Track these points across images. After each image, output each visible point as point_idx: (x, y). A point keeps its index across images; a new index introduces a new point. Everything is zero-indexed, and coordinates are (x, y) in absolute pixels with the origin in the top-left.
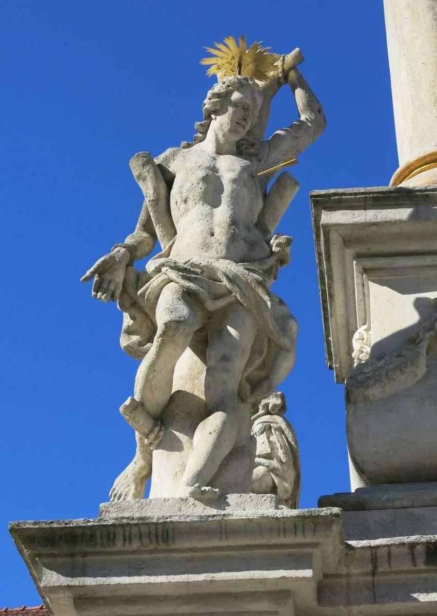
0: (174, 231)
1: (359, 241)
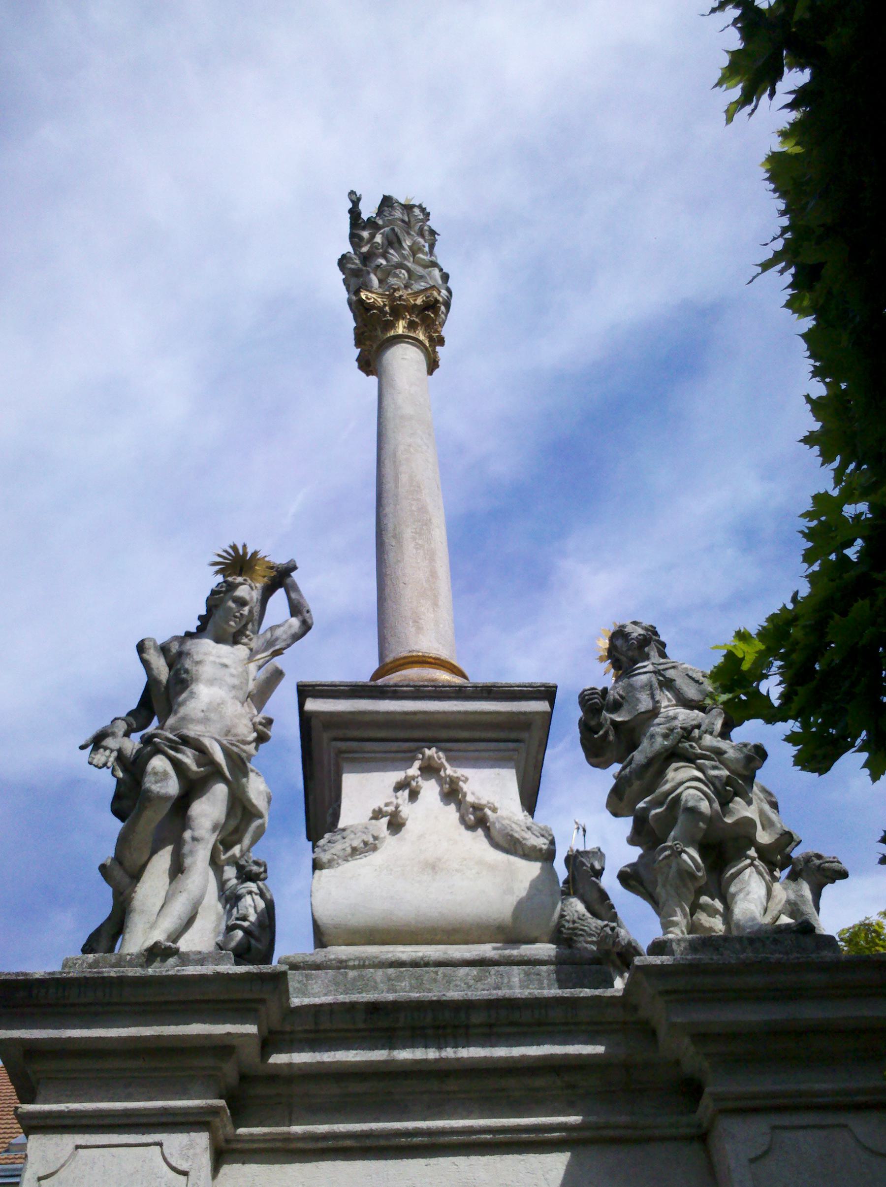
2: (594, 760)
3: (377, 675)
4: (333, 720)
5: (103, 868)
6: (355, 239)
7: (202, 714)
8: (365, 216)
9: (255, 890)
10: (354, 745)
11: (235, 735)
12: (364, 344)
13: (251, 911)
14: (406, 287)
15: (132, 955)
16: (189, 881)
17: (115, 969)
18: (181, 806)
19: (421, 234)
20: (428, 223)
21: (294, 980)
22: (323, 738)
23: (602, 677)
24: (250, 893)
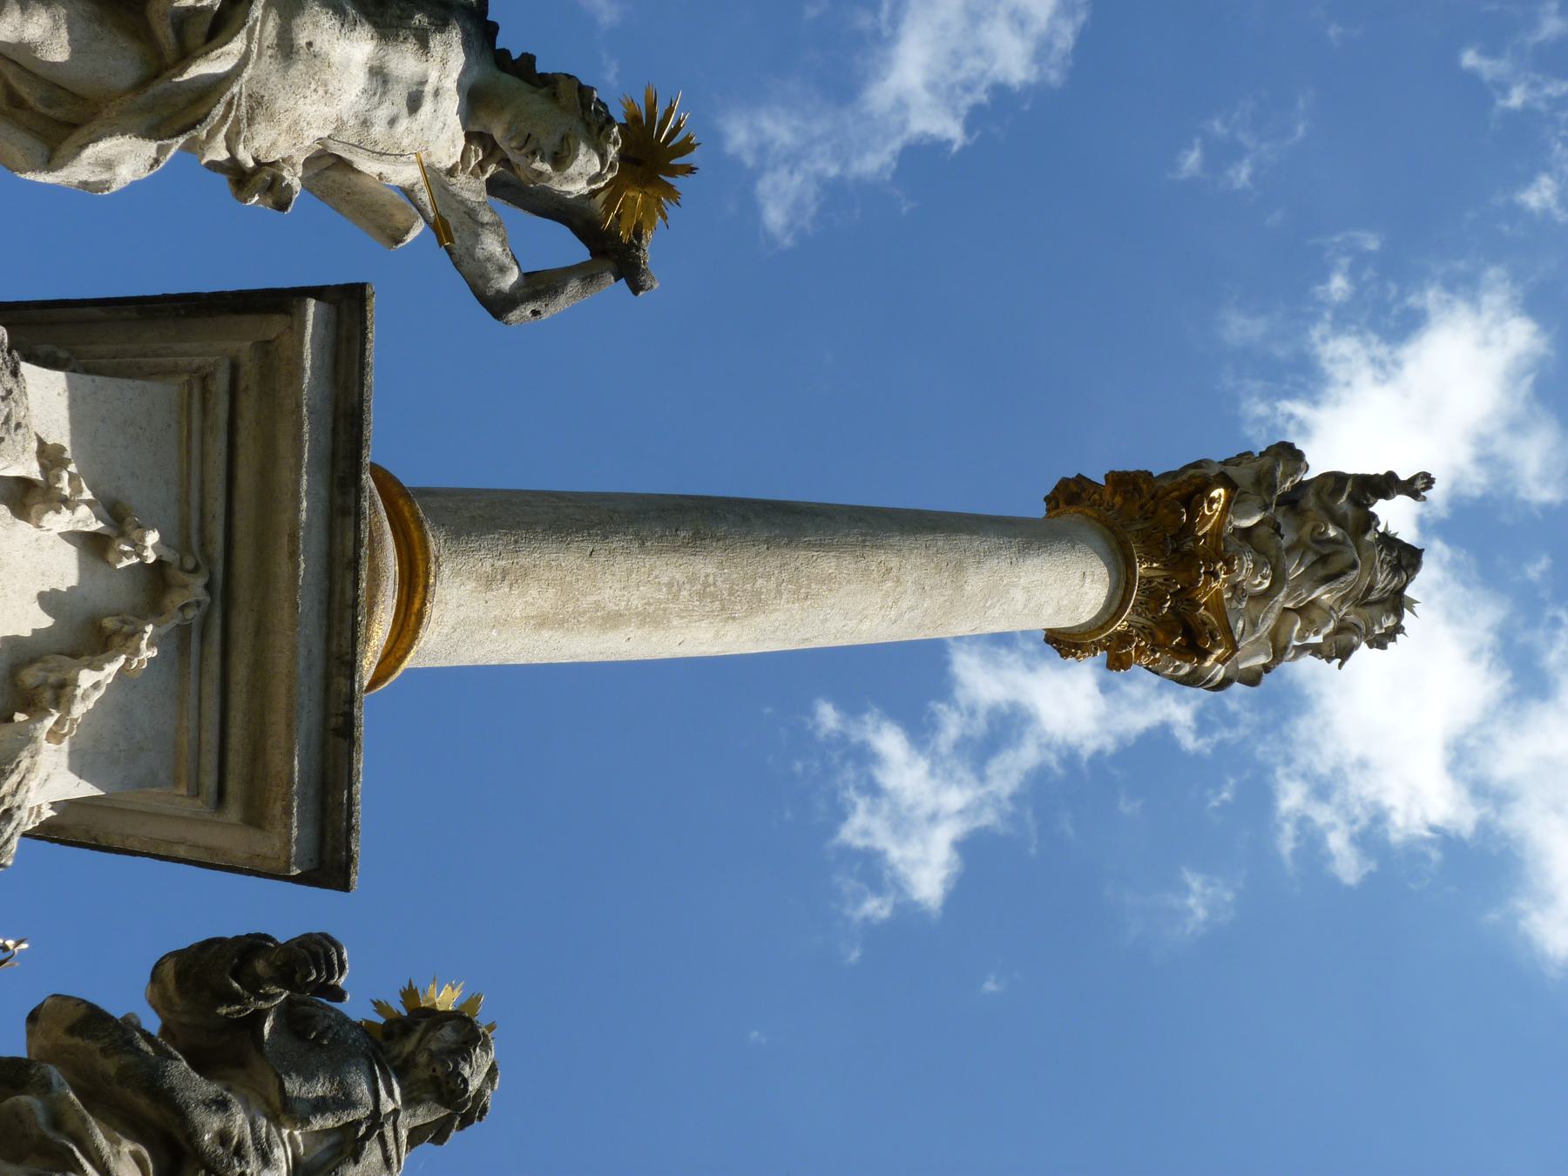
2: (169, 970)
3: (384, 480)
4: (275, 362)
6: (1335, 481)
7: (302, 40)
8: (1381, 508)
10: (221, 411)
11: (251, 120)
12: (1114, 494)
14: (1234, 587)
19: (1342, 628)
20: (1364, 645)
22: (236, 342)
23: (363, 995)
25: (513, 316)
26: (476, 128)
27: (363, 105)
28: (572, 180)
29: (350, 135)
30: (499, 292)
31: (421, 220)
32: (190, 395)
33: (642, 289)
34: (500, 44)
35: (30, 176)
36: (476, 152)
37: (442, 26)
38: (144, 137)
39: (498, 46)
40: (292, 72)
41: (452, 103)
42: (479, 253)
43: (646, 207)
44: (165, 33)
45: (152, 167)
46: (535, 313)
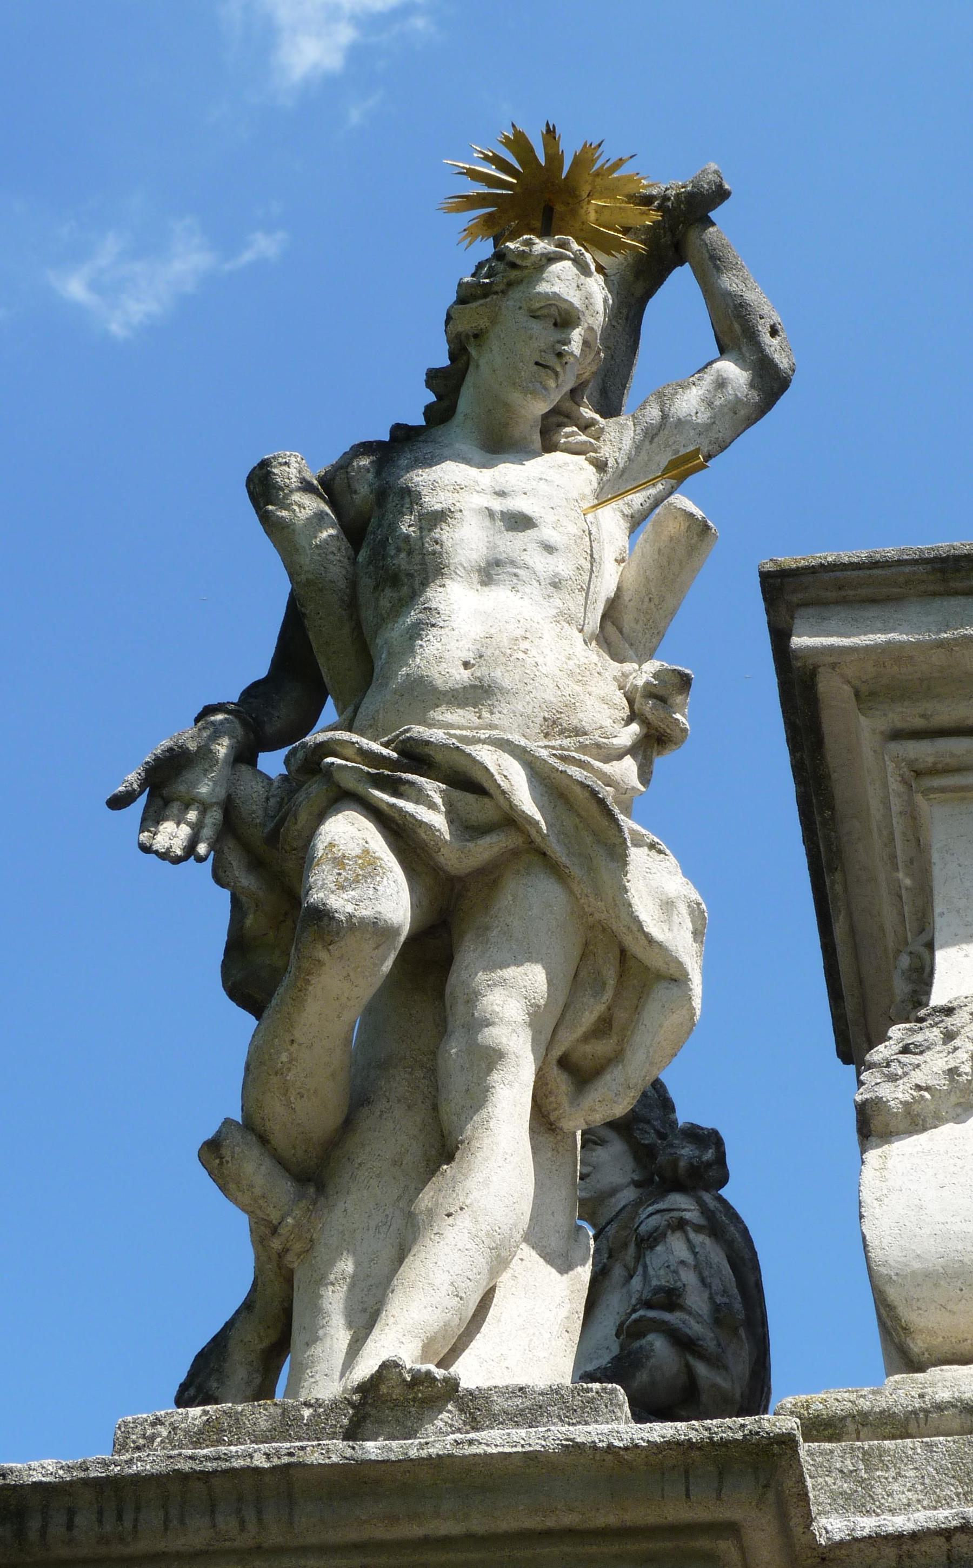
0: (272, 1336)
1: (899, 692)
4: (882, 684)
5: (212, 1152)
7: (462, 676)
9: (693, 1215)
11: (578, 732)
13: (689, 1278)
15: (318, 1404)
16: (472, 1183)
17: (264, 1447)
18: (432, 959)
21: (822, 1469)
22: (859, 737)
24: (681, 1225)
25: (782, 361)
26: (537, 437)
27: (533, 590)
28: (588, 297)
29: (575, 603)
30: (752, 385)
31: (672, 499)
32: (943, 790)
33: (720, 186)
34: (418, 419)
35: (697, 1003)
36: (568, 436)
37: (410, 496)
38: (625, 864)
39: (422, 422)
40: (506, 683)
41: (508, 473)
42: (703, 417)
43: (609, 192)
44: (486, 849)
45: (660, 852)
46: (774, 332)
